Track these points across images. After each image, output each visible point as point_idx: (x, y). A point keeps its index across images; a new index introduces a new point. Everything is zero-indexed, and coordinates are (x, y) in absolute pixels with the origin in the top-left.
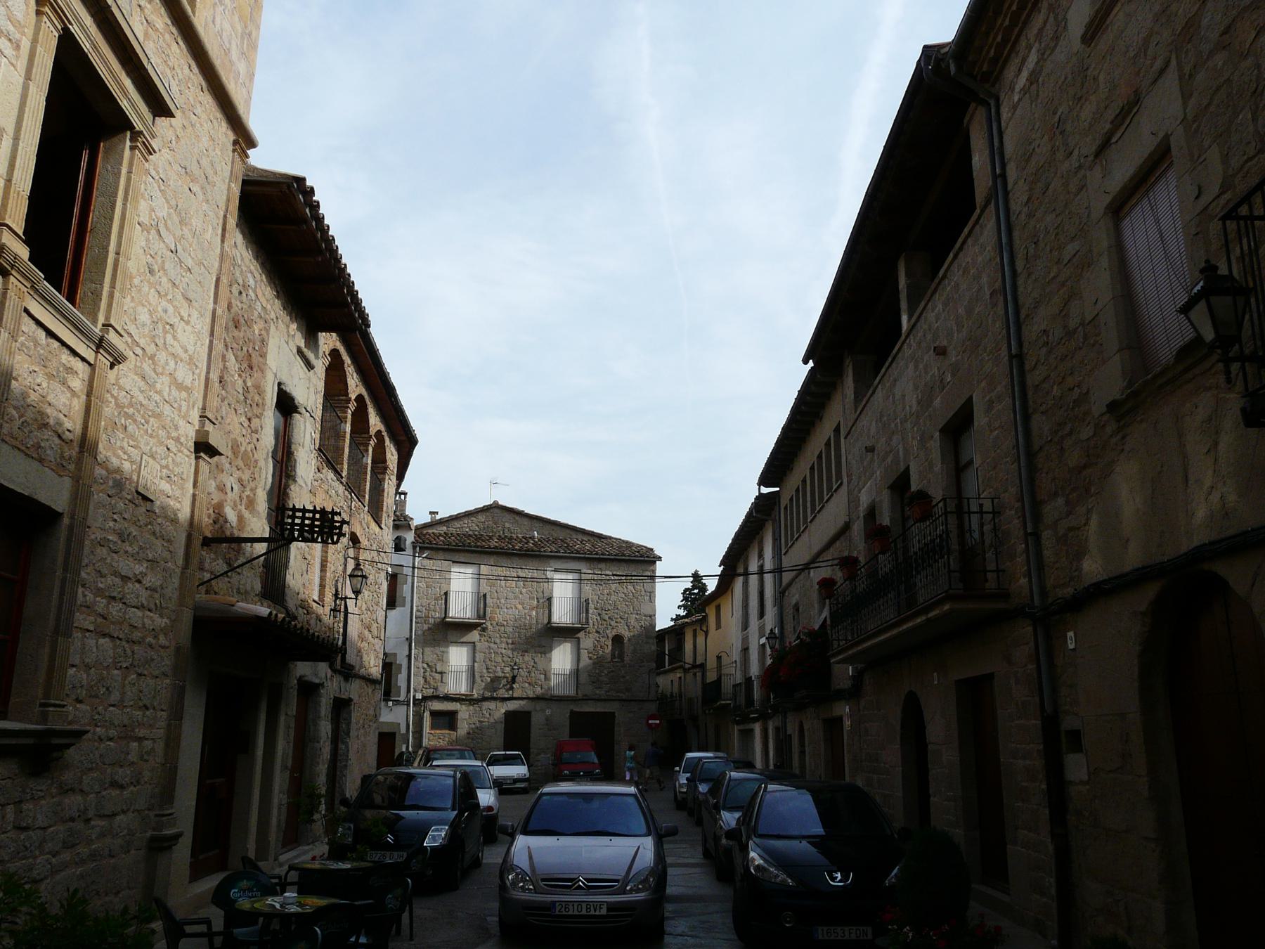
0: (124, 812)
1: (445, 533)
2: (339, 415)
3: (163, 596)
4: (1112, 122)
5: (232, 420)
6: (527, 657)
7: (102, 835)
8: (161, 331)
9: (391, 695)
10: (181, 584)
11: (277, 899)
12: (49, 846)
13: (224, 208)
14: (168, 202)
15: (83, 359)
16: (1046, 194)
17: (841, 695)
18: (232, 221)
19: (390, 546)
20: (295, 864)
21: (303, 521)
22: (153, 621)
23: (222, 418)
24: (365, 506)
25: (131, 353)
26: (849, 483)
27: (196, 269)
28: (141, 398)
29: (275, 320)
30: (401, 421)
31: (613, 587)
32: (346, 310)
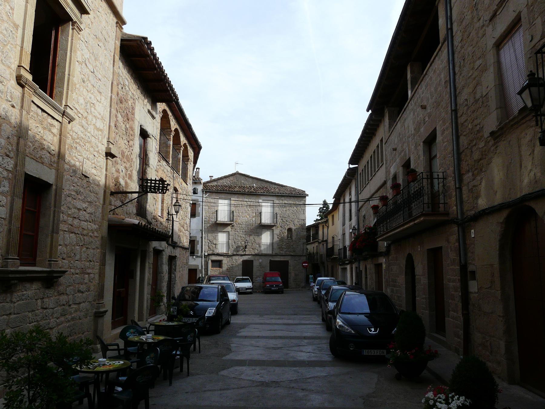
0: (84, 302)
3: (95, 216)
4: (497, 6)
5: (121, 142)
7: (76, 311)
8: (89, 106)
10: (102, 211)
11: (144, 336)
12: (55, 315)
13: (113, 52)
14: (89, 51)
15: (57, 120)
16: (469, 38)
17: (381, 254)
18: (117, 57)
19: (191, 192)
20: (153, 323)
22: (92, 226)
23: (117, 142)
25: (77, 116)
27: (102, 79)
28: (82, 135)
29: (138, 99)
30: (194, 139)
31: (288, 208)
32: (168, 93)
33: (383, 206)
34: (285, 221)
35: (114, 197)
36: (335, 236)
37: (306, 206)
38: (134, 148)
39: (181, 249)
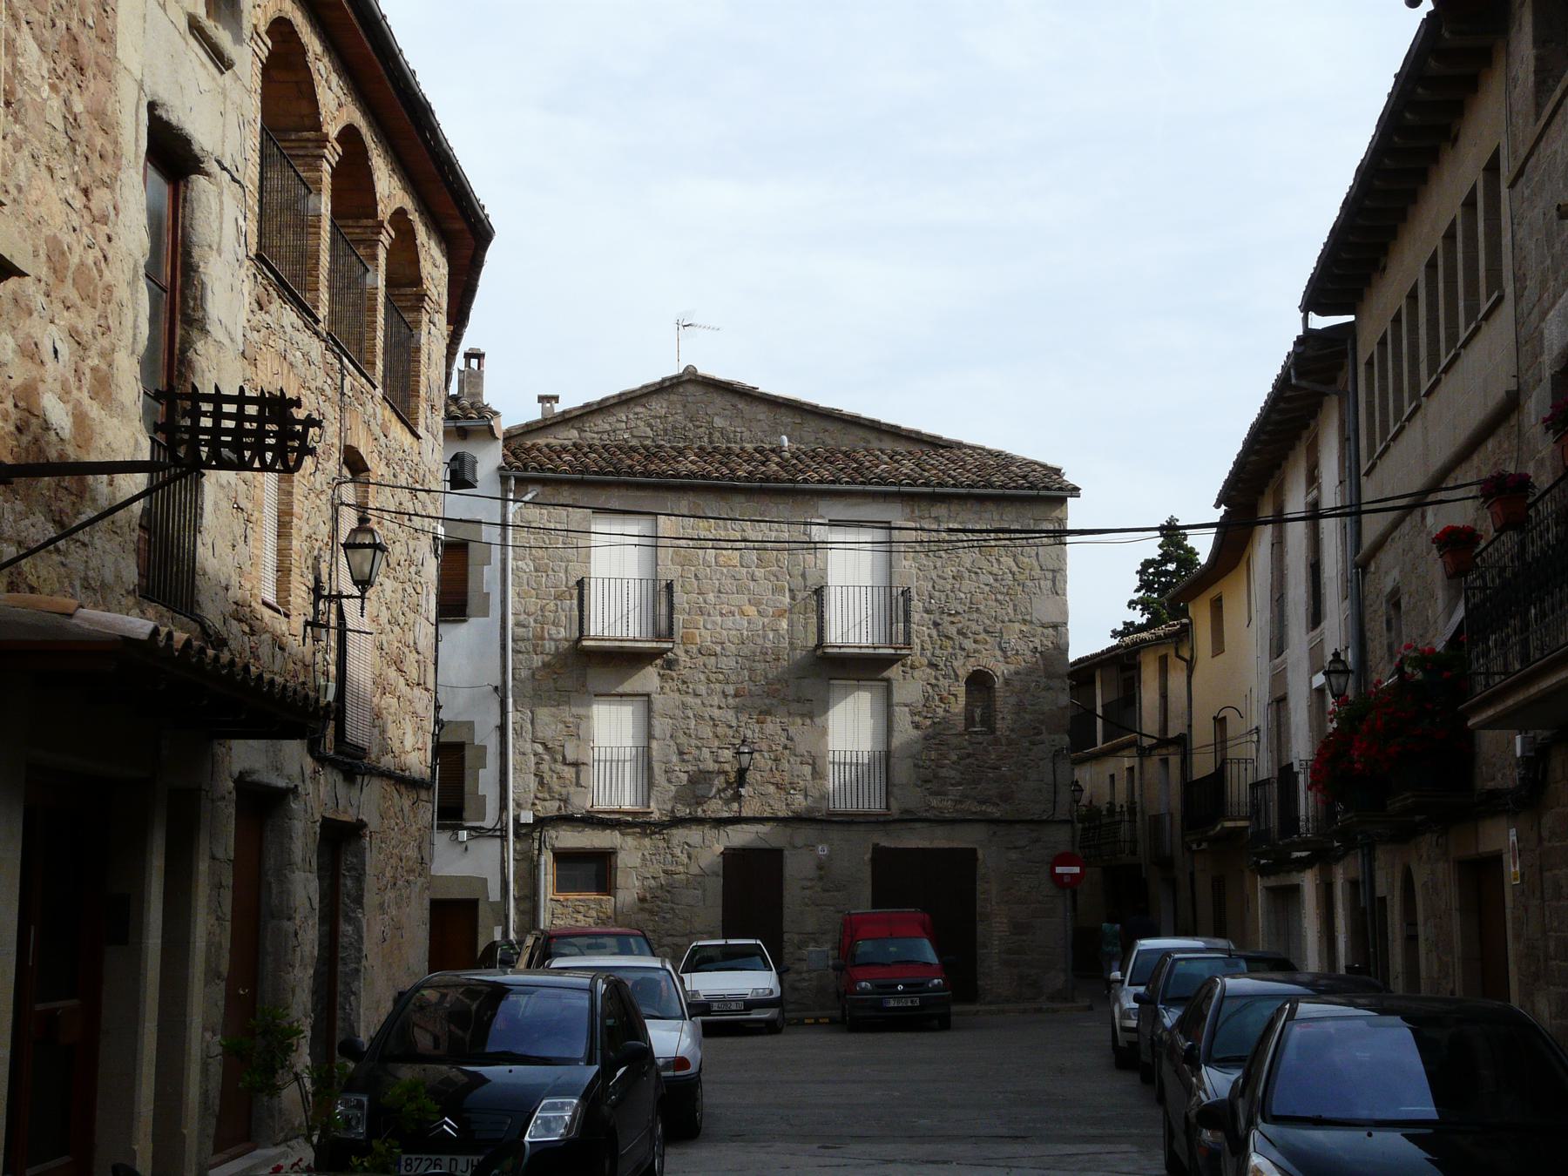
1: (574, 445)
2: (303, 175)
5: (44, 193)
6: (771, 726)
9: (466, 815)
17: (1496, 804)
21: (217, 423)
23: (19, 189)
24: (375, 387)
26: (1518, 298)
30: (449, 185)
33: (1500, 531)
34: (952, 631)
35: (15, 492)
36: (1231, 715)
37: (1069, 539)
38: (121, 230)
39: (390, 788)
